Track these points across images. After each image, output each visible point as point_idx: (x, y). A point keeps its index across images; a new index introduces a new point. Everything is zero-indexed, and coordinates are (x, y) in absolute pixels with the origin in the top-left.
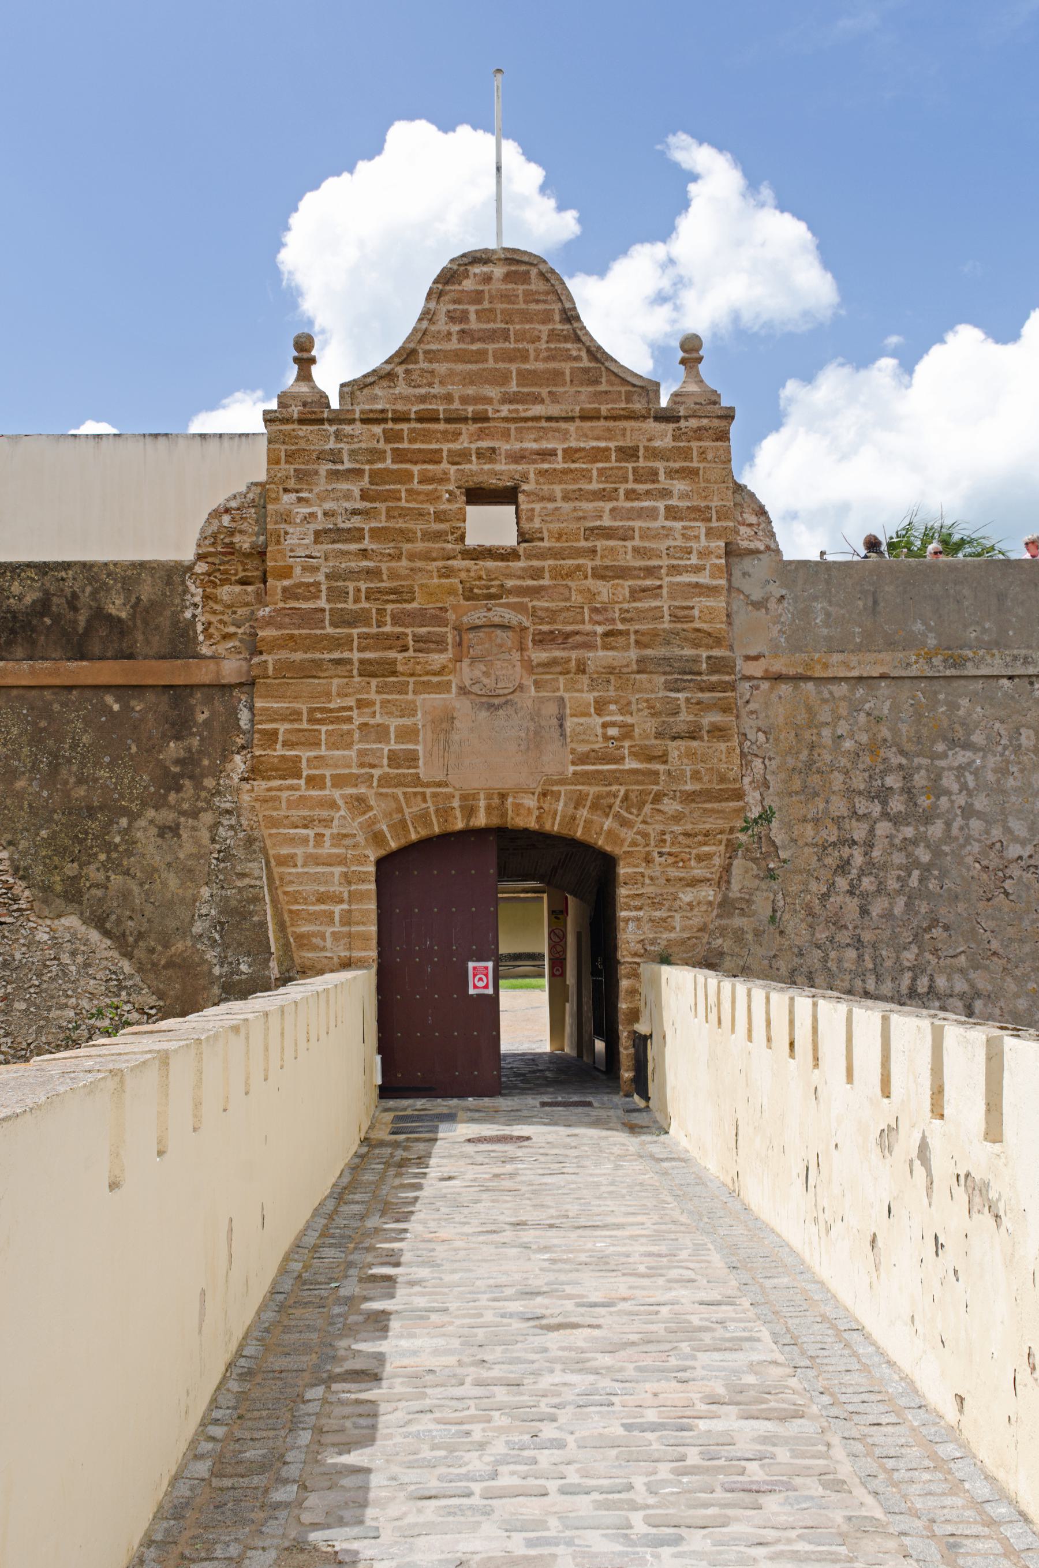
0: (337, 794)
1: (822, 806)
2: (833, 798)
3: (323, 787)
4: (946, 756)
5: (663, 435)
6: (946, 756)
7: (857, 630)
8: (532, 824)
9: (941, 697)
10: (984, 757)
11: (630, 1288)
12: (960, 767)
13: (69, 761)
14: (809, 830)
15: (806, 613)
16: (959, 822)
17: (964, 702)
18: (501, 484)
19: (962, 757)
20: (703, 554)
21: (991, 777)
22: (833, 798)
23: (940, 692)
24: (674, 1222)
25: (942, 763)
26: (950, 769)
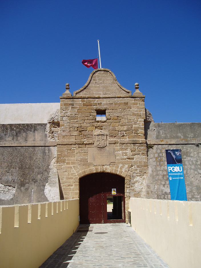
0: (72, 166)
1: (163, 168)
2: (165, 166)
3: (70, 164)
4: (186, 158)
5: (132, 101)
6: (186, 158)
7: (168, 135)
8: (95, 172)
9: (185, 147)
10: (193, 158)
11: (93, 266)
12: (189, 160)
13: (10, 159)
14: (161, 172)
15: (159, 132)
16: (189, 170)
17: (189, 148)
18: (103, 109)
19: (189, 158)
20: (140, 121)
21: (194, 162)
22: (165, 166)
23: (184, 147)
24: (93, 255)
25: (186, 160)
26: (187, 161)
